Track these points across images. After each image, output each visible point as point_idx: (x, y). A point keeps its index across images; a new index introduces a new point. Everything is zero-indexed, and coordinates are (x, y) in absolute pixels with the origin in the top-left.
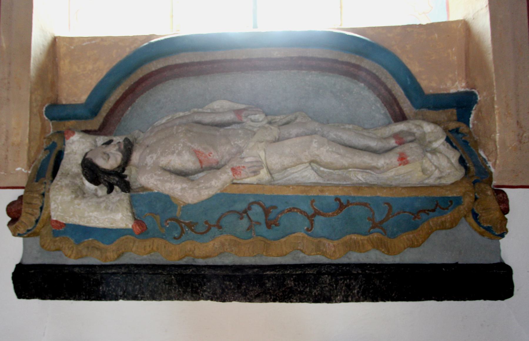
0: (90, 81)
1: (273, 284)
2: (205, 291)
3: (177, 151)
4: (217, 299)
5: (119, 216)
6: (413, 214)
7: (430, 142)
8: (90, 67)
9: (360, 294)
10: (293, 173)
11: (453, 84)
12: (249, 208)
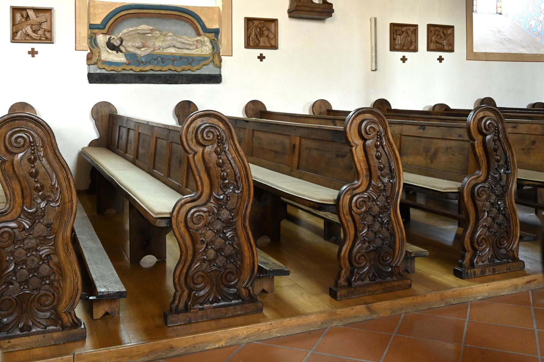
8: (100, 11)
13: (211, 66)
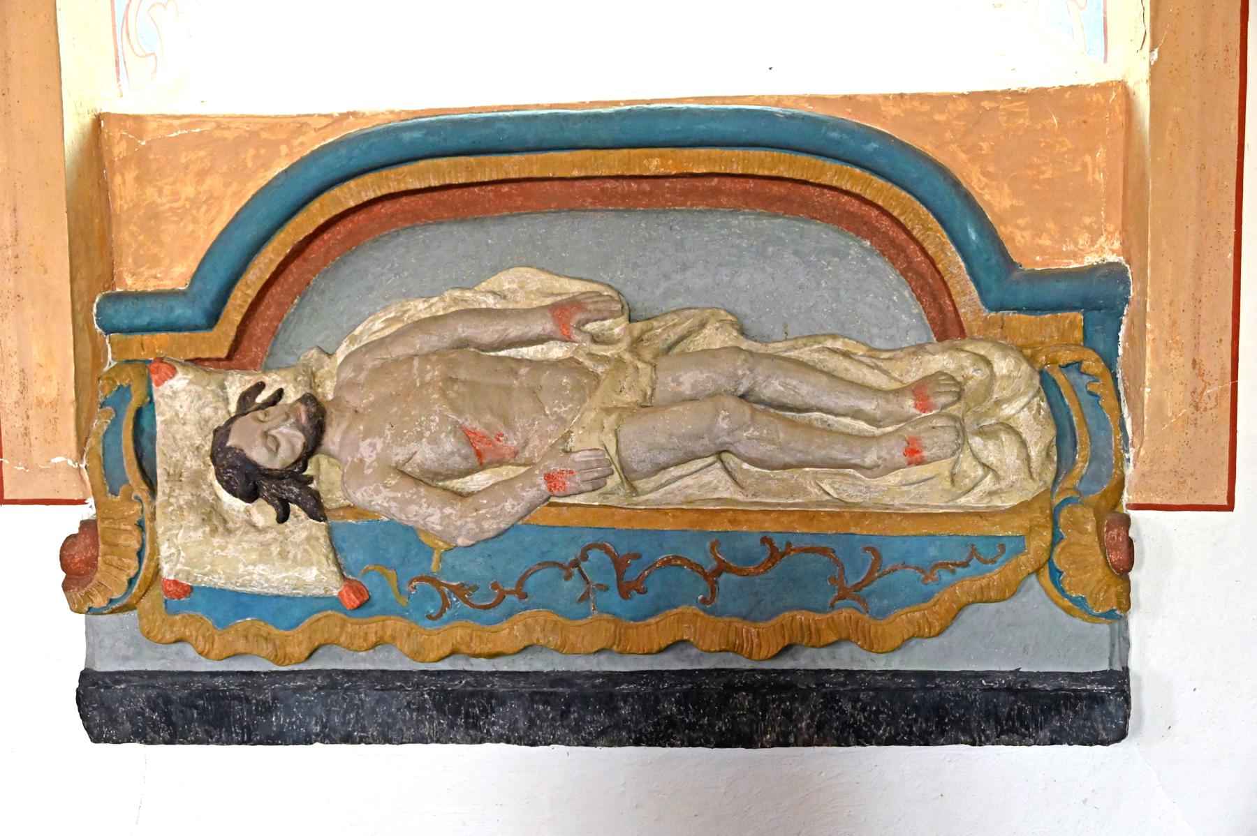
0: (191, 227)
1: (633, 709)
2: (494, 724)
3: (427, 434)
4: (519, 741)
5: (311, 574)
6: (923, 572)
7: (998, 403)
8: (189, 191)
9: (812, 730)
10: (681, 477)
11: (1093, 242)
12: (584, 557)
13: (1035, 598)
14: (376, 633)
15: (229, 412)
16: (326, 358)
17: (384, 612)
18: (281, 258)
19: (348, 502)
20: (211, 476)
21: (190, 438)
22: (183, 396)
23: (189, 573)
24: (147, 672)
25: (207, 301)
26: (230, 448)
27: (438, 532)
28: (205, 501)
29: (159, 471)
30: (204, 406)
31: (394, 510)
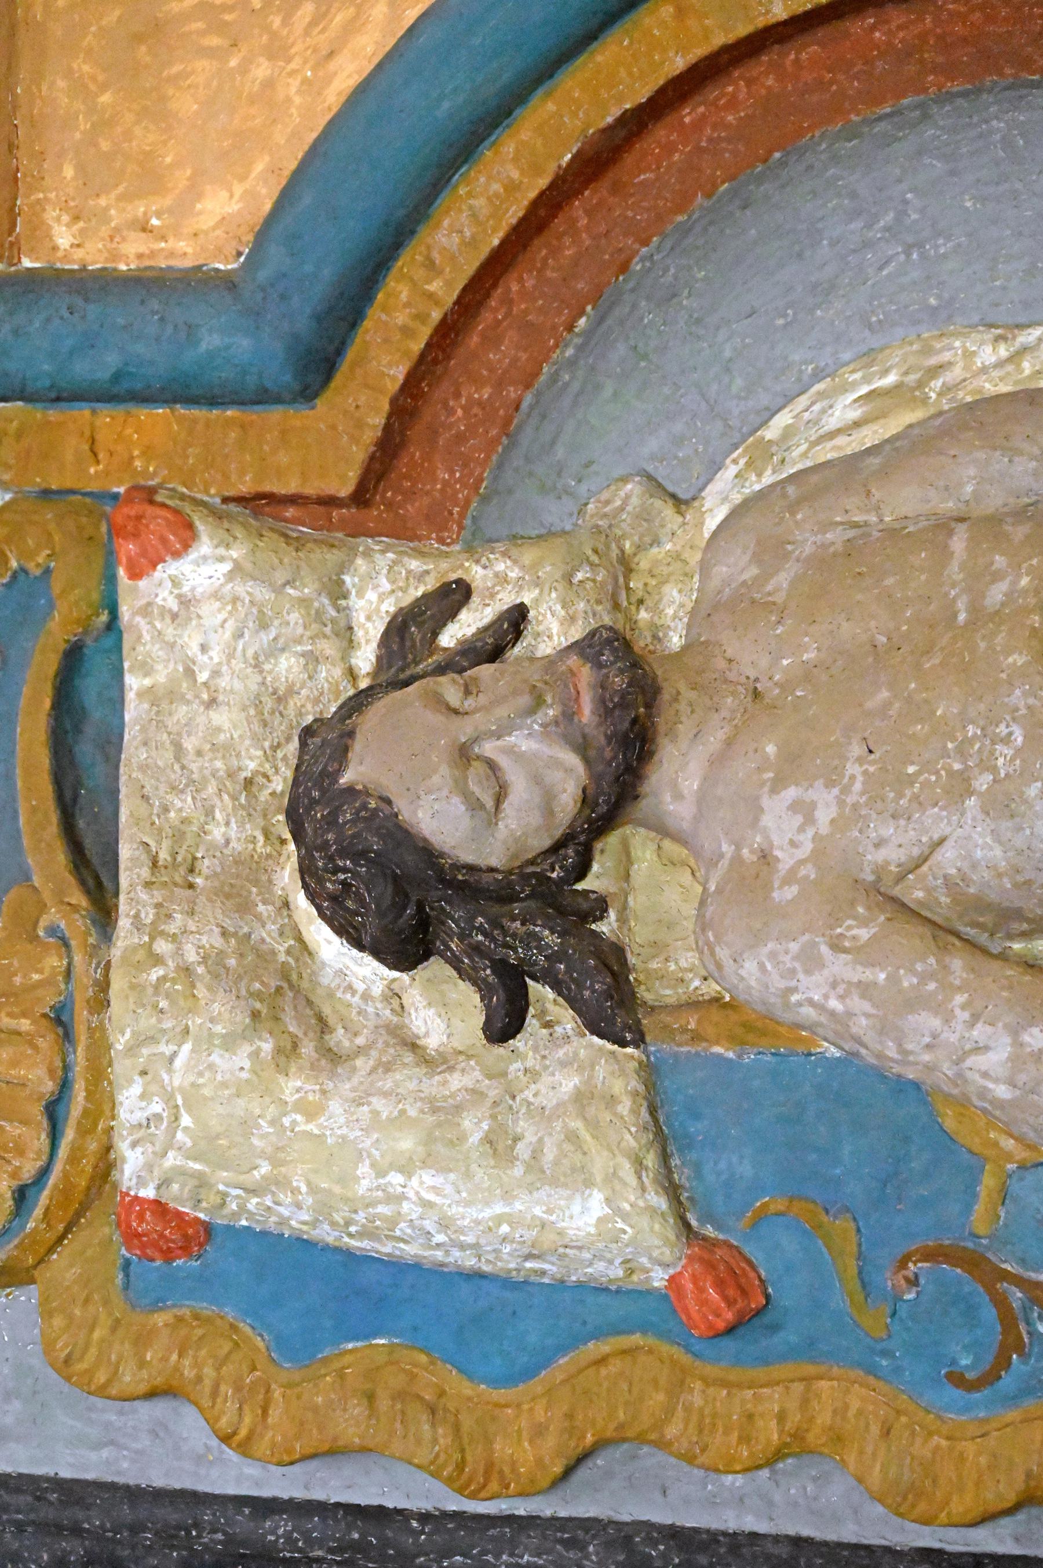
0: (262, 70)
14: (781, 1417)
15: (352, 674)
16: (668, 511)
17: (808, 1350)
18: (543, 182)
19: (712, 988)
20: (287, 876)
21: (227, 749)
22: (212, 614)
23: (202, 1182)
24: (58, 1484)
25: (300, 314)
26: (350, 791)
27: (1000, 1104)
28: (265, 956)
29: (125, 852)
30: (275, 650)
31: (861, 1025)
